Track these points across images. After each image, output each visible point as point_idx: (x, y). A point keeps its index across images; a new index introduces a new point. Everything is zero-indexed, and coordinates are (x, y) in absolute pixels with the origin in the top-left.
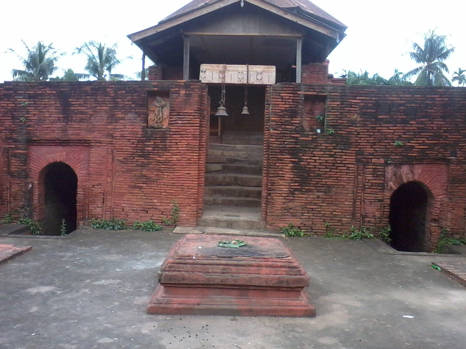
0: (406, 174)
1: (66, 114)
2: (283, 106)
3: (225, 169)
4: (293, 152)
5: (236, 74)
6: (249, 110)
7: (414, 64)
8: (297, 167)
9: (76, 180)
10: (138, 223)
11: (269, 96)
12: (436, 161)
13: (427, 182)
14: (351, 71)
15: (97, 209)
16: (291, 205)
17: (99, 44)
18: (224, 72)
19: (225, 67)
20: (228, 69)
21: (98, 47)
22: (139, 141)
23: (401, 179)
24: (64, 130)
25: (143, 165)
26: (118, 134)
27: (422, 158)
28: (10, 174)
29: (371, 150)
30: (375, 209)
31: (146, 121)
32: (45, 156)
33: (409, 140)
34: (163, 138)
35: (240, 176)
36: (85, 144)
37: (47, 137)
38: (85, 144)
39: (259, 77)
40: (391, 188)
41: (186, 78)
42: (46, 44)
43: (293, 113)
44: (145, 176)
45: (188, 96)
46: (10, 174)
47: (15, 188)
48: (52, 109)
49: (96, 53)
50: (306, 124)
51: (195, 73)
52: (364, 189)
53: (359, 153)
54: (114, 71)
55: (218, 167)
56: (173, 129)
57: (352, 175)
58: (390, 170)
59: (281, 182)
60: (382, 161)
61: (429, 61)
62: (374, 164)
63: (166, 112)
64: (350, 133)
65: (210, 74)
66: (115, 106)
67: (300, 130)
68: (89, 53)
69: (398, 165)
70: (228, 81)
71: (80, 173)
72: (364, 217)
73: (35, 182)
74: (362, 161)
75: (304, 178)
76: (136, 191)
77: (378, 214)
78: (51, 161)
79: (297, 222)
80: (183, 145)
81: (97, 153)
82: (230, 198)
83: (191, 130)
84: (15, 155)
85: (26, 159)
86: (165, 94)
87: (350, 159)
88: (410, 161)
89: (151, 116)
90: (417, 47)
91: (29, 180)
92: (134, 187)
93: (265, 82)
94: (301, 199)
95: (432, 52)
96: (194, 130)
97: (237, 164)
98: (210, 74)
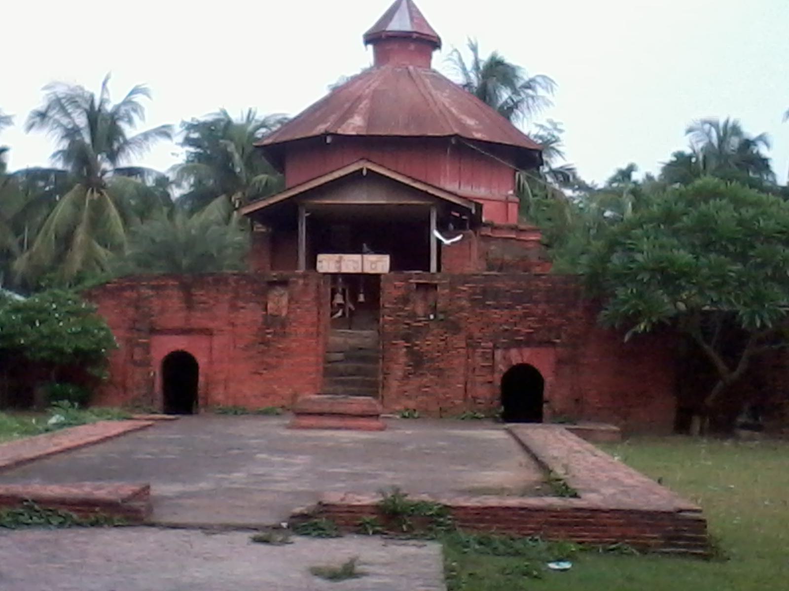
0: (516, 357)
1: (189, 304)
4: (407, 338)
5: (351, 263)
6: (365, 297)
12: (541, 344)
13: (536, 364)
15: (219, 395)
17: (90, 102)
19: (341, 258)
21: (87, 107)
22: (259, 329)
23: (511, 362)
25: (263, 352)
27: (529, 341)
28: (135, 363)
29: (480, 335)
30: (487, 390)
31: (266, 309)
32: (165, 346)
33: (515, 324)
34: (283, 325)
36: (208, 332)
38: (208, 332)
39: (373, 266)
40: (501, 370)
41: (302, 269)
43: (406, 300)
45: (306, 285)
46: (135, 363)
48: (175, 300)
49: (81, 121)
51: (312, 263)
53: (470, 337)
55: (340, 356)
57: (463, 360)
58: (499, 354)
59: (396, 366)
60: (491, 344)
62: (484, 348)
63: (285, 301)
64: (459, 319)
66: (237, 297)
67: (413, 315)
69: (507, 348)
70: (344, 270)
71: (202, 360)
72: (475, 398)
73: (156, 372)
74: (472, 344)
75: (417, 362)
76: (257, 376)
77: (488, 396)
79: (411, 404)
80: (302, 330)
81: (218, 341)
82: (352, 389)
84: (138, 344)
85: (147, 348)
86: (284, 283)
87: (459, 341)
88: (518, 344)
94: (415, 382)
96: (311, 317)
97: (362, 353)
98: (327, 263)
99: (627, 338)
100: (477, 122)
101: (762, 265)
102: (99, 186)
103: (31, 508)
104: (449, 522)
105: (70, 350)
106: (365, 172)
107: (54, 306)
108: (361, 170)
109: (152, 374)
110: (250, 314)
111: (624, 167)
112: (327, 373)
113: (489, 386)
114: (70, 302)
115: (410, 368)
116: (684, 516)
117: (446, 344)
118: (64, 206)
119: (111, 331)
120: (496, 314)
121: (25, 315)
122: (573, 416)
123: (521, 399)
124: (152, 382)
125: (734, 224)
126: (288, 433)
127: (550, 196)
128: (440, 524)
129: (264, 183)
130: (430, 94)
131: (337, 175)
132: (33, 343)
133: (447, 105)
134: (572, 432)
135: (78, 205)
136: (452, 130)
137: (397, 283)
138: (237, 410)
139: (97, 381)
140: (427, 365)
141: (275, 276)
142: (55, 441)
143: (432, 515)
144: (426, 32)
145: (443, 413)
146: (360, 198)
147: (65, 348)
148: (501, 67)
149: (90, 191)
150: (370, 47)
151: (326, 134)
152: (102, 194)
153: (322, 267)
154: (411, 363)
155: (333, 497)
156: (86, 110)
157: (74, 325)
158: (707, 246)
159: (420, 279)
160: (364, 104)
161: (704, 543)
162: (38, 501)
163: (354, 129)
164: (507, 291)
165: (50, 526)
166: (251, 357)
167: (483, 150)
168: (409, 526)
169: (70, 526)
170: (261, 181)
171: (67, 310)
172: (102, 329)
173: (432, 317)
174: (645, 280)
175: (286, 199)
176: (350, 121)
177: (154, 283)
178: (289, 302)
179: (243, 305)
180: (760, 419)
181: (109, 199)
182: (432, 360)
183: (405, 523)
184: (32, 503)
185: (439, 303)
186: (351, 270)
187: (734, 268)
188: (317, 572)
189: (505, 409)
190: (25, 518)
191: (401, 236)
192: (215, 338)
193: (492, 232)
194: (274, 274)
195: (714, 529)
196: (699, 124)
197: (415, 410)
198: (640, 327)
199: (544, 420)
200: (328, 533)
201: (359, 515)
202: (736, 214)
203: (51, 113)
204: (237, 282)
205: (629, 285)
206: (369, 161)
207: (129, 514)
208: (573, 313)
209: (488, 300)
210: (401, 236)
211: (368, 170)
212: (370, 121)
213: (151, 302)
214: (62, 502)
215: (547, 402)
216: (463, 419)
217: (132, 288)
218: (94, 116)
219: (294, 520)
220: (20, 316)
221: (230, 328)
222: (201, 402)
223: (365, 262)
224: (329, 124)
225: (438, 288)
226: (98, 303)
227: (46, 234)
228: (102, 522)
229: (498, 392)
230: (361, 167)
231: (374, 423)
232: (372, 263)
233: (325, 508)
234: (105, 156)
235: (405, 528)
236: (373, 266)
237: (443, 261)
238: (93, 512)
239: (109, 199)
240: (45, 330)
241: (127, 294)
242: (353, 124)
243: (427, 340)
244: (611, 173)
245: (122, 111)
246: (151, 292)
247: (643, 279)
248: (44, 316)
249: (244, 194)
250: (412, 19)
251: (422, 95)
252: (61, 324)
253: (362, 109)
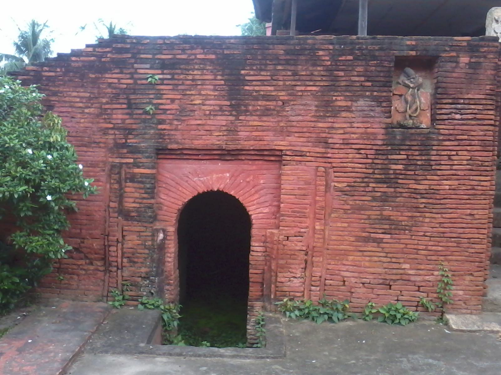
15: (292, 280)
24: (232, 131)
25: (385, 199)
26: (336, 139)
28: (126, 215)
36: (275, 157)
37: (198, 143)
38: (275, 157)
44: (388, 218)
46: (126, 215)
48: (208, 90)
56: (444, 128)
63: (424, 98)
66: (333, 85)
71: (258, 211)
73: (168, 230)
76: (371, 247)
78: (202, 189)
81: (294, 176)
84: (132, 178)
85: (151, 185)
86: (426, 63)
91: (158, 225)
92: (366, 240)
109: (161, 236)
124: (162, 247)
141: (412, 48)
166: (360, 209)
172: (50, 147)
192: (287, 169)
196: (265, 34)
213: (159, 95)
217: (120, 65)
222: (254, 291)
241: (112, 77)
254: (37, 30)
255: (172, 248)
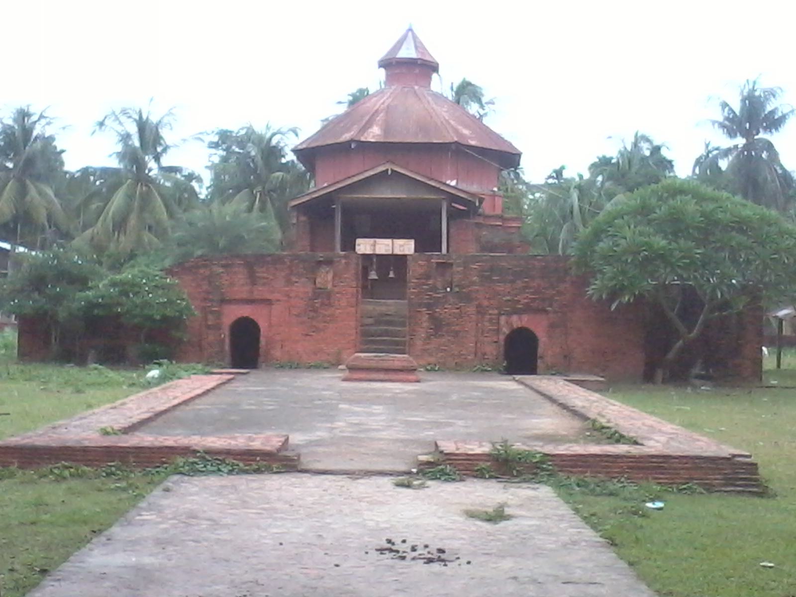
0: (517, 322)
1: (253, 280)
2: (422, 271)
3: (378, 323)
4: (429, 306)
5: (383, 246)
7: (724, 142)
8: (432, 317)
9: (259, 330)
10: (309, 363)
11: (411, 265)
14: (639, 135)
15: (277, 353)
16: (427, 347)
18: (374, 245)
20: (377, 242)
21: (137, 117)
23: (512, 326)
24: (251, 292)
25: (313, 318)
26: (292, 295)
27: (528, 309)
30: (493, 349)
35: (391, 328)
36: (268, 302)
37: (237, 297)
38: (268, 302)
42: (35, 111)
44: (315, 326)
47: (211, 338)
49: (133, 129)
50: (439, 285)
51: (349, 245)
52: (483, 333)
53: (479, 306)
54: (166, 161)
55: (370, 321)
56: (336, 289)
57: (474, 324)
58: (503, 319)
60: (496, 312)
61: (747, 134)
62: (490, 314)
63: (330, 277)
65: (364, 246)
67: (434, 289)
68: (120, 129)
69: (509, 314)
70: (378, 252)
71: (263, 325)
74: (481, 311)
75: (437, 326)
78: (239, 316)
79: (432, 360)
80: (344, 303)
81: (277, 309)
83: (350, 290)
84: (212, 312)
85: (219, 315)
86: (329, 262)
87: (471, 309)
89: (318, 280)
90: (727, 109)
91: (221, 331)
92: (307, 335)
93: (407, 252)
94: (435, 342)
95: (753, 117)
97: (388, 318)
98: (364, 246)
99: (613, 307)
100: (471, 132)
101: (721, 249)
102: (149, 181)
103: (204, 458)
104: (551, 467)
105: (158, 317)
106: (390, 172)
107: (144, 281)
108: (387, 170)
109: (223, 336)
110: (302, 287)
111: (558, 167)
112: (365, 334)
113: (495, 344)
114: (157, 278)
115: (431, 331)
116: (738, 461)
117: (461, 311)
118: (118, 199)
119: (190, 301)
120: (500, 287)
121: (121, 289)
122: (564, 367)
123: (520, 356)
124: (223, 341)
125: (699, 215)
126: (346, 384)
127: (509, 190)
128: (543, 470)
129: (280, 179)
130: (433, 108)
131: (371, 173)
132: (128, 312)
133: (447, 118)
134: (577, 384)
135: (130, 197)
136: (453, 139)
137: (420, 262)
138: (294, 365)
139: (180, 341)
140: (445, 329)
141: (321, 257)
142: (171, 394)
143: (537, 462)
144: (427, 58)
145: (457, 366)
146: (386, 193)
147: (155, 316)
148: (470, 88)
149: (140, 184)
150: (382, 71)
151: (352, 141)
152: (149, 187)
153: (359, 250)
154: (432, 327)
155: (448, 447)
156: (135, 120)
157: (161, 296)
158: (676, 234)
159: (439, 259)
160: (380, 117)
161: (757, 483)
162: (208, 452)
163: (374, 137)
164: (509, 269)
165: (221, 473)
167: (480, 155)
168: (518, 471)
169: (237, 473)
170: (278, 178)
171: (154, 284)
172: (183, 299)
173: (448, 289)
174: (629, 261)
175: (326, 194)
176: (370, 130)
177: (223, 262)
178: (333, 278)
179: (297, 280)
180: (711, 370)
181: (154, 191)
182: (448, 324)
183: (514, 469)
184: (204, 455)
185: (455, 278)
186: (383, 252)
187: (699, 251)
188: (472, 515)
189: (508, 363)
190: (200, 467)
191: (416, 221)
192: (273, 307)
193: (484, 220)
194: (321, 255)
195: (763, 472)
197: (435, 365)
198: (625, 298)
199: (538, 371)
200: (453, 477)
201: (475, 462)
202: (698, 207)
203: (106, 122)
204: (291, 261)
205: (615, 265)
206: (393, 163)
207: (281, 462)
208: (562, 287)
209: (717, 296)
210: (416, 221)
211: (392, 171)
212: (386, 130)
214: (228, 453)
215: (541, 357)
216: (475, 371)
217: (205, 266)
218: (142, 126)
219: (422, 467)
220: (117, 289)
221: (286, 298)
223: (395, 245)
224: (352, 133)
225: (454, 266)
226: (179, 278)
227: (105, 220)
228: (263, 469)
229: (502, 349)
230: (384, 169)
231: (411, 377)
232: (401, 246)
233: (448, 457)
234: (151, 157)
235: (515, 473)
236: (402, 249)
237: (451, 244)
238: (254, 460)
239: (154, 191)
240: (138, 301)
242: (372, 132)
243: (445, 308)
244: (549, 171)
245: (165, 121)
246: (221, 270)
247: (627, 260)
248: (137, 289)
249: (264, 188)
250: (416, 47)
251: (427, 110)
252: (150, 295)
253: (379, 120)
254: (28, 122)
255: (227, 341)
